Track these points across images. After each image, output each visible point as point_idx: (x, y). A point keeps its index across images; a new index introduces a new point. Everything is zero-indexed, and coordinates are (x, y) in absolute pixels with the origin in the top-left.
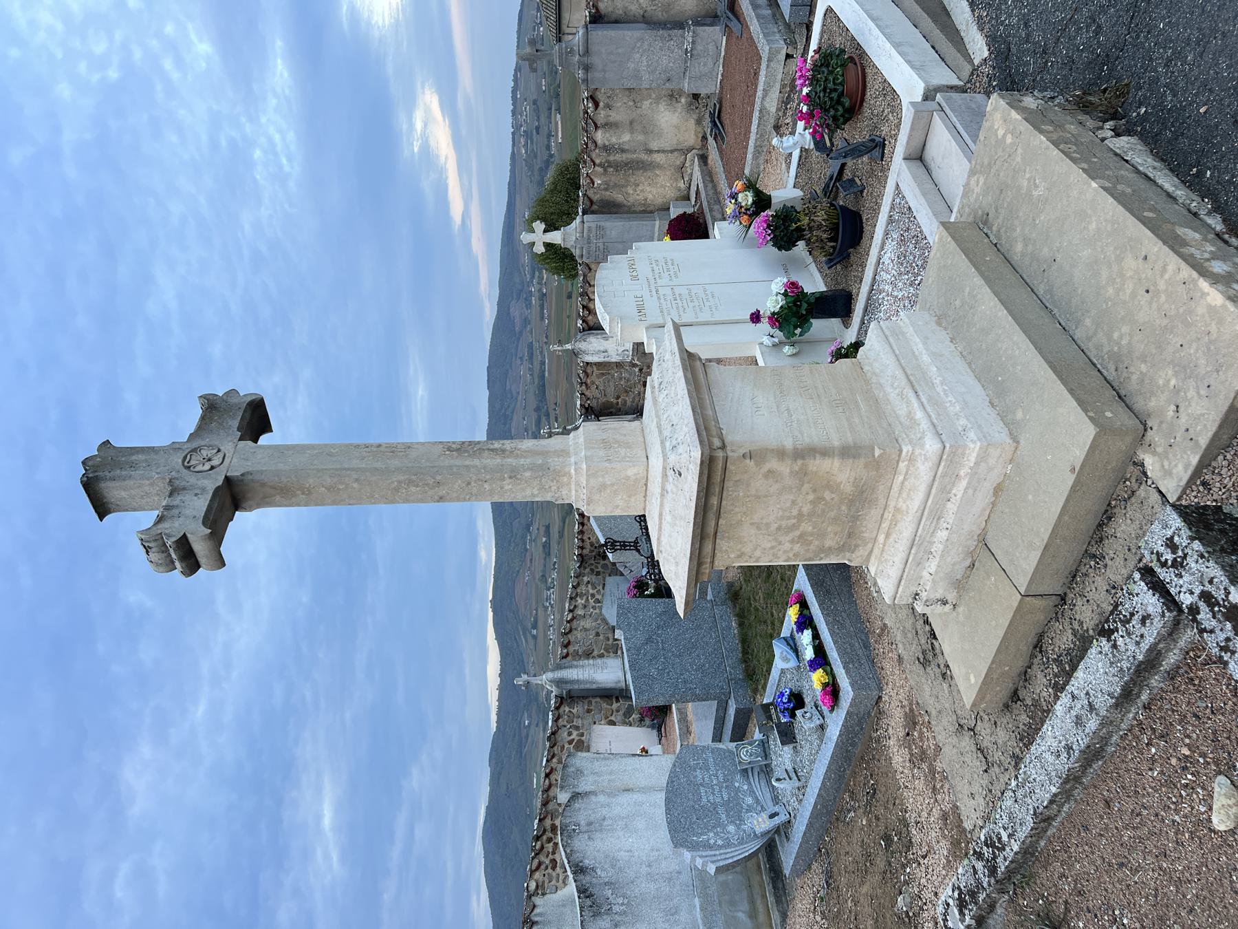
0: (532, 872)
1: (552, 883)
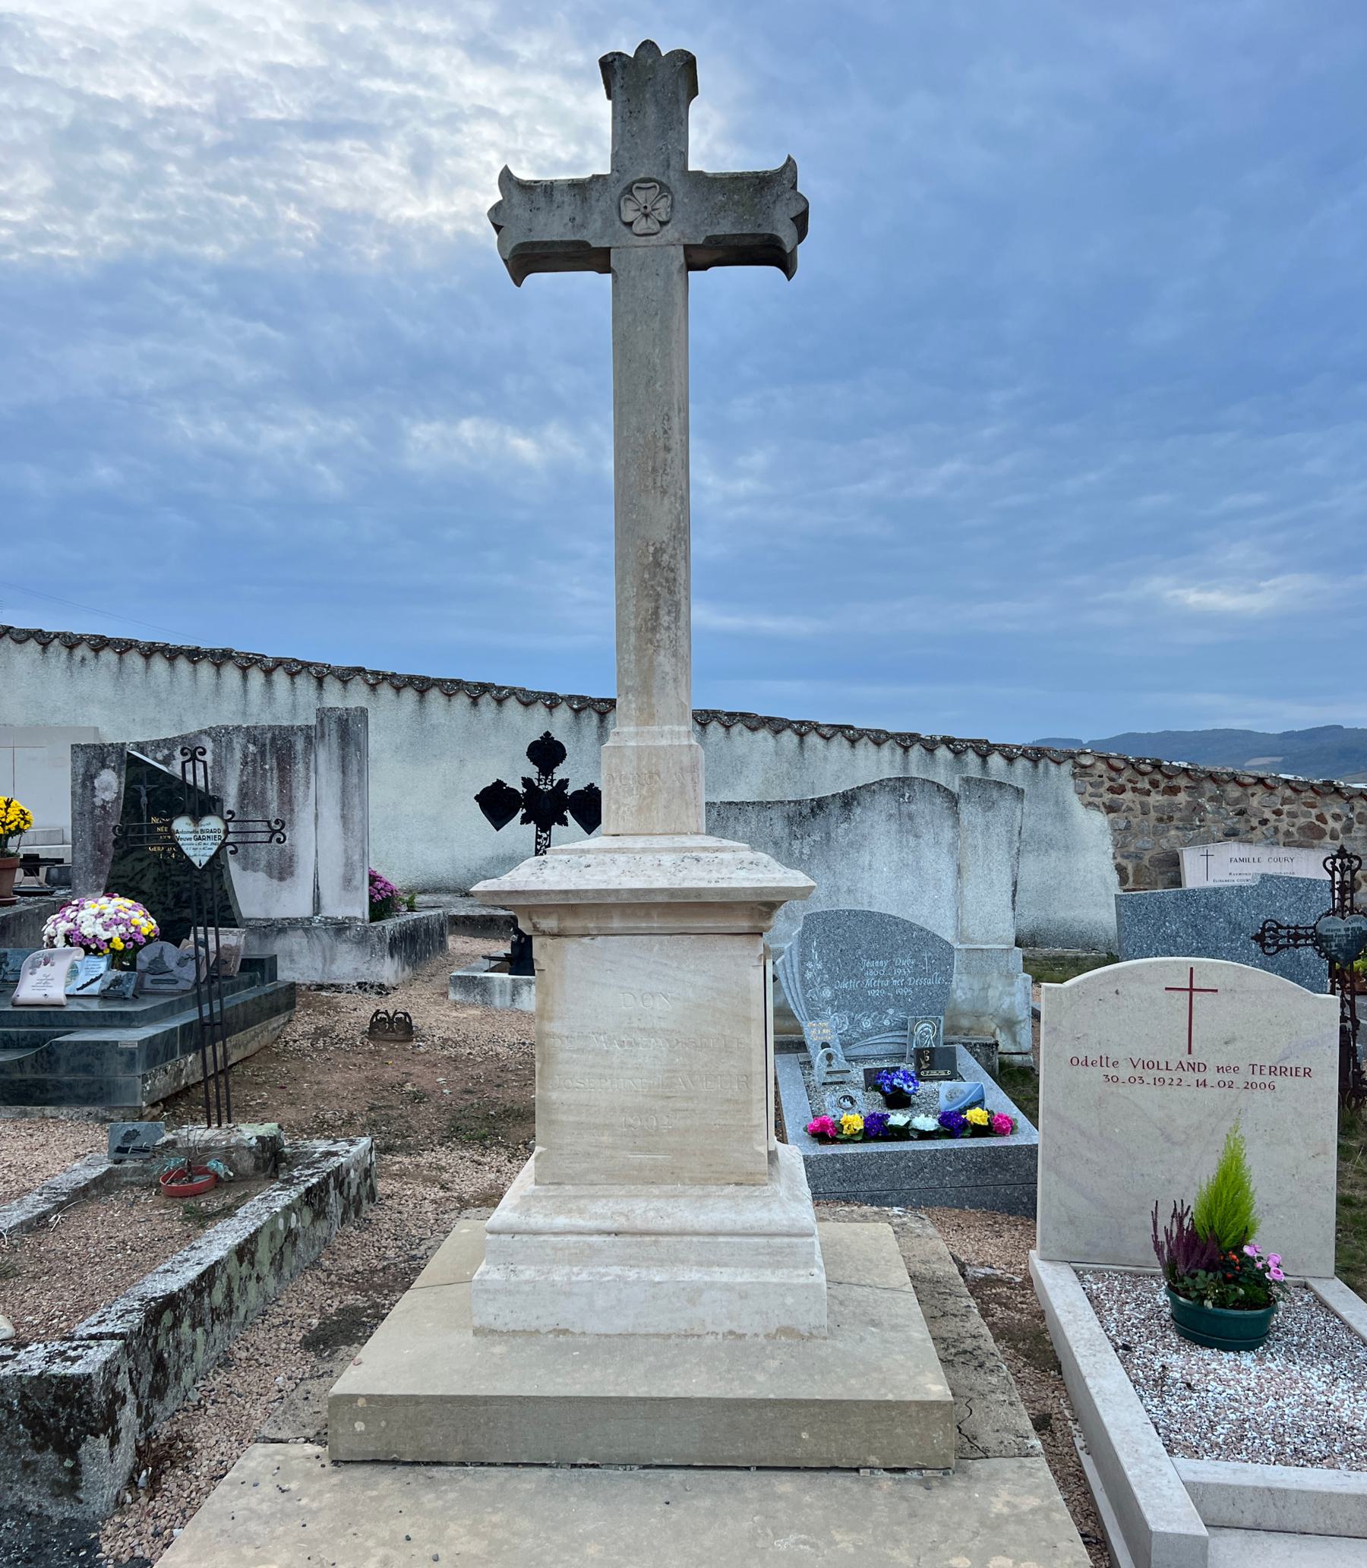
0: (1106, 759)
1: (1089, 787)
